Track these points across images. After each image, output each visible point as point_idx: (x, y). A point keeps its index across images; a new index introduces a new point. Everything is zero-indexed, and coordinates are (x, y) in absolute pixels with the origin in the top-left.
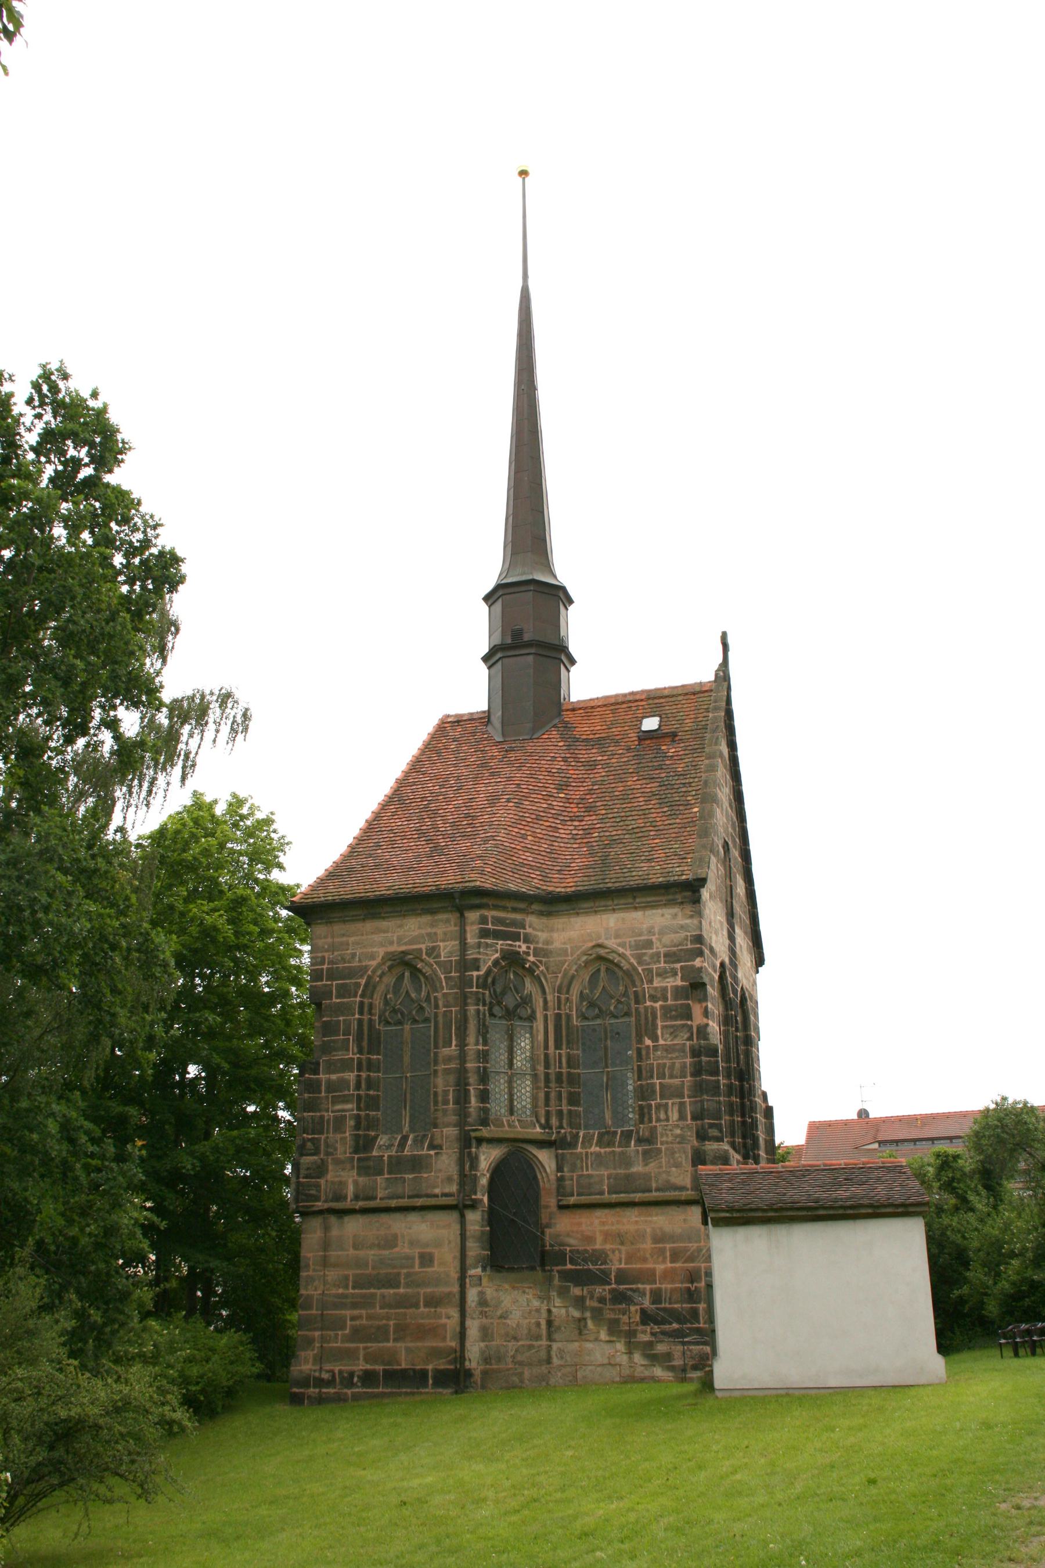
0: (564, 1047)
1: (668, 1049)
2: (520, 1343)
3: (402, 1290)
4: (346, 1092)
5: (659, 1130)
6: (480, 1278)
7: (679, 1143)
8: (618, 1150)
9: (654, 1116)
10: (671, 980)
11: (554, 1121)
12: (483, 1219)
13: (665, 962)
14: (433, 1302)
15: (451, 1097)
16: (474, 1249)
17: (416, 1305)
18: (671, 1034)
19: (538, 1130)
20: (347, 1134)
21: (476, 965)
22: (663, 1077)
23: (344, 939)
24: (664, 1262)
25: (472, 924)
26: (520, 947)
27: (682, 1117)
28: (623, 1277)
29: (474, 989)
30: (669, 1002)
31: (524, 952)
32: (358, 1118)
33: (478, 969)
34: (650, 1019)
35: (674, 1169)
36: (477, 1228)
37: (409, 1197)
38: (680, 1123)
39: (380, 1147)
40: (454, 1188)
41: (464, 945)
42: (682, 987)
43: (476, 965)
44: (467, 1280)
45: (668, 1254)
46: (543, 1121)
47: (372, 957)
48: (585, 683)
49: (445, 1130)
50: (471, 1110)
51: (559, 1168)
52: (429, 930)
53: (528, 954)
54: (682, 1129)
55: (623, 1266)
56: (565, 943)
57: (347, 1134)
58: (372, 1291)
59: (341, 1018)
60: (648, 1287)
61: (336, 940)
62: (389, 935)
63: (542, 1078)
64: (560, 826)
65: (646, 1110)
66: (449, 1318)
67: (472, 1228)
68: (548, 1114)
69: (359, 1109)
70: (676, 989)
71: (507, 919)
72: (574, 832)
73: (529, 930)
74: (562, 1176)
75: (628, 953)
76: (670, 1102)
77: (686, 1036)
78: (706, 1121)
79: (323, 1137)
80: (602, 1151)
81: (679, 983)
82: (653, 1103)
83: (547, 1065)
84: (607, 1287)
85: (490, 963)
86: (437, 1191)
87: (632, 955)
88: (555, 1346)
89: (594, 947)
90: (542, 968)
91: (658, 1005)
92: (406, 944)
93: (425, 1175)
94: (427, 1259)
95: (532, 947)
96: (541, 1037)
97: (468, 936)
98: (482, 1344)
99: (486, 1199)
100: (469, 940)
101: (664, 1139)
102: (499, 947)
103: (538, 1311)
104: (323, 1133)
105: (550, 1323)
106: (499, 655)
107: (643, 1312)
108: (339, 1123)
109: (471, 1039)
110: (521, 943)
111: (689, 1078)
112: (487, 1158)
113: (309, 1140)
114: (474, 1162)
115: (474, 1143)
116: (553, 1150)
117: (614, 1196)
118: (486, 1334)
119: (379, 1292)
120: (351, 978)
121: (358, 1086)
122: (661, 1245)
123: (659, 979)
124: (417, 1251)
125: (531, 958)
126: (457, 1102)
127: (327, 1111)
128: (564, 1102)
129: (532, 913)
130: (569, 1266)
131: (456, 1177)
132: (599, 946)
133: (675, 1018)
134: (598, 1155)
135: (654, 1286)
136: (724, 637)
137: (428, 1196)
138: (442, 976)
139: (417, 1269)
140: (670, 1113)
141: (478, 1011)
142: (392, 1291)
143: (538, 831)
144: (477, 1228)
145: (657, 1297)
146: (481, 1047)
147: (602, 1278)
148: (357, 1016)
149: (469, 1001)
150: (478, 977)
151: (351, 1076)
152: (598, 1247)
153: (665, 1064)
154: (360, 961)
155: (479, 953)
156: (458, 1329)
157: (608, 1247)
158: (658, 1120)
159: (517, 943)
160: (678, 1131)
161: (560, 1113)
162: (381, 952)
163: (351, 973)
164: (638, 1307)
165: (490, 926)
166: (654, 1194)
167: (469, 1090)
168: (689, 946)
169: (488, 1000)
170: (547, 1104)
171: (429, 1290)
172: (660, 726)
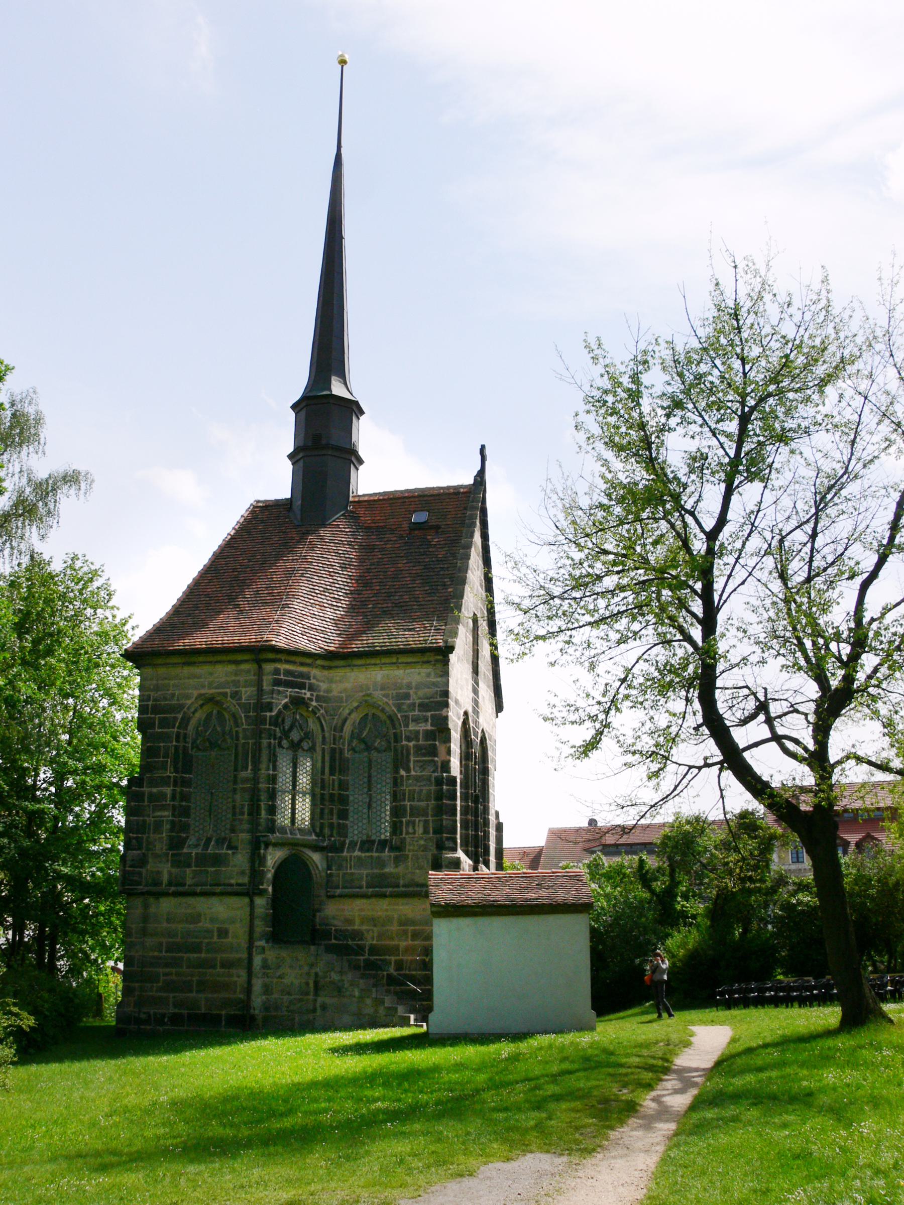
1: (417, 779)
3: (203, 955)
5: (408, 840)
6: (263, 948)
8: (375, 854)
12: (268, 904)
14: (227, 965)
15: (246, 810)
16: (260, 927)
17: (214, 967)
18: (421, 767)
19: (314, 837)
23: (166, 682)
24: (406, 940)
26: (305, 694)
27: (426, 831)
28: (374, 950)
31: (309, 699)
33: (271, 710)
39: (189, 846)
40: (245, 880)
42: (432, 731)
46: (318, 830)
52: (234, 678)
53: (311, 700)
54: (426, 840)
55: (374, 942)
59: (162, 745)
61: (160, 682)
65: (398, 825)
68: (322, 825)
69: (173, 815)
73: (313, 681)
75: (391, 702)
76: (417, 820)
79: (145, 836)
80: (363, 855)
81: (429, 727)
82: (404, 820)
83: (323, 788)
84: (362, 958)
85: (280, 707)
86: (233, 881)
87: (394, 704)
91: (411, 744)
96: (319, 765)
97: (265, 684)
99: (270, 889)
100: (265, 688)
106: (301, 455)
109: (263, 766)
112: (273, 857)
114: (263, 860)
115: (263, 846)
118: (267, 990)
121: (173, 798)
125: (314, 703)
127: (149, 816)
128: (335, 817)
130: (333, 941)
131: (247, 872)
133: (424, 755)
134: (359, 858)
136: (483, 449)
137: (224, 885)
142: (196, 955)
144: (262, 910)
145: (399, 966)
149: (263, 735)
150: (271, 717)
151: (168, 790)
152: (356, 927)
153: (414, 791)
154: (178, 700)
157: (364, 928)
158: (408, 833)
159: (303, 691)
160: (422, 842)
162: (195, 693)
165: (282, 677)
168: (439, 699)
170: (322, 817)
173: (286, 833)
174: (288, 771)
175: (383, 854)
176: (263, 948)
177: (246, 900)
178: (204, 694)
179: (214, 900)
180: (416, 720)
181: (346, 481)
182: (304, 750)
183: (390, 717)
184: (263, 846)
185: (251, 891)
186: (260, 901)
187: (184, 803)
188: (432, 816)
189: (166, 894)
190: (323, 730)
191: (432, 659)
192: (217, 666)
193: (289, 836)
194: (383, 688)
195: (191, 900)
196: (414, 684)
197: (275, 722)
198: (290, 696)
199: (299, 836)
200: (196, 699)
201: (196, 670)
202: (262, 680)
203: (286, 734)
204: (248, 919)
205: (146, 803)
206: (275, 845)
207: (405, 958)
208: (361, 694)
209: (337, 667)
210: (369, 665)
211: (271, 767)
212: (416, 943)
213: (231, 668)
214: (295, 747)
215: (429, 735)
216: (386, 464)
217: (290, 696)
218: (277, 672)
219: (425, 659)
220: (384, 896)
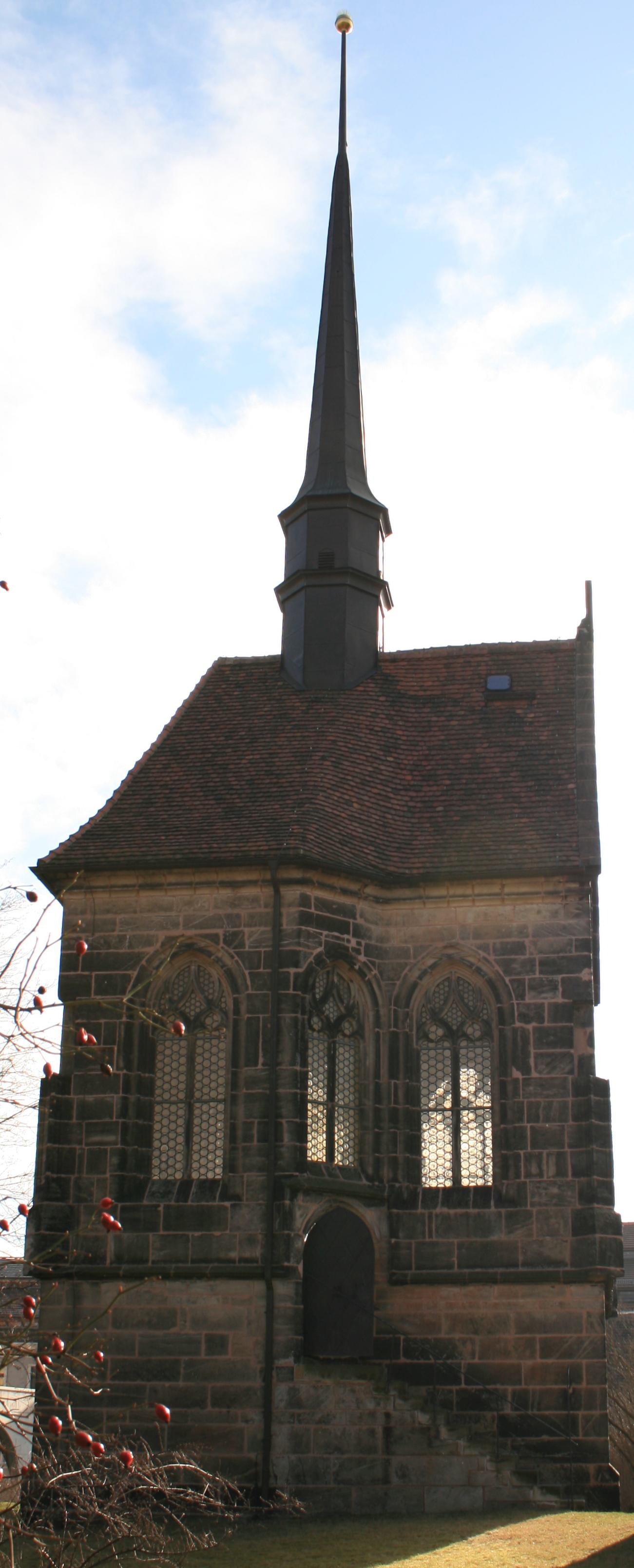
0: (401, 1076)
1: (543, 1084)
2: (345, 1456)
3: (181, 1384)
4: (107, 1120)
5: (529, 1188)
6: (291, 1370)
7: (556, 1205)
8: (472, 1211)
9: (522, 1169)
10: (550, 995)
11: (386, 1172)
12: (297, 1294)
13: (541, 972)
14: (225, 1400)
15: (255, 1132)
16: (285, 1334)
17: (201, 1404)
18: (548, 1065)
19: (364, 1182)
20: (108, 1175)
21: (294, 959)
22: (537, 1120)
23: (109, 916)
24: (532, 1356)
25: (290, 905)
26: (348, 941)
27: (560, 1172)
28: (475, 1373)
29: (291, 991)
30: (546, 1024)
31: (354, 949)
32: (123, 1155)
33: (296, 965)
34: (520, 1043)
35: (548, 1238)
36: (289, 1304)
37: (193, 1261)
38: (557, 1179)
39: (153, 1194)
40: (257, 1252)
41: (278, 933)
42: (564, 1005)
43: (294, 959)
44: (274, 1373)
45: (538, 1347)
46: (370, 1171)
47: (149, 942)
48: (400, 631)
49: (245, 1175)
50: (283, 1150)
51: (393, 1233)
52: (229, 911)
53: (358, 951)
54: (560, 1187)
55: (476, 1360)
56: (406, 942)
57: (108, 1175)
58: (139, 1382)
59: (102, 1021)
60: (510, 1388)
61: (98, 917)
62: (173, 914)
63: (371, 1115)
64: (392, 795)
65: (511, 1162)
66: (247, 1421)
67: (282, 1304)
68: (378, 1163)
69: (124, 1141)
70: (556, 1007)
71: (334, 903)
72: (410, 804)
73: (359, 921)
74: (396, 1243)
75: (492, 958)
76: (545, 1152)
77: (567, 1068)
78: (595, 1177)
79: (73, 1177)
80: (452, 1212)
81: (560, 1000)
82: (522, 1152)
83: (378, 1099)
84: (454, 1388)
85: (311, 959)
86: (233, 1255)
87: (497, 961)
88: (395, 1461)
89: (445, 947)
90: (375, 972)
91: (530, 1027)
92: (196, 927)
93: (217, 1233)
94: (217, 1344)
95: (363, 943)
96: (370, 1062)
97: (284, 921)
98: (293, 1457)
99: (300, 1268)
100: (285, 927)
101: (536, 1199)
102: (323, 938)
103: (372, 1414)
104: (73, 1173)
105: (388, 1431)
106: (302, 583)
107: (503, 1419)
108: (96, 1160)
109: (286, 1056)
110: (350, 937)
111: (571, 1123)
112: (306, 1212)
113: (54, 1180)
114: (288, 1218)
115: (288, 1192)
116: (384, 1209)
117: (466, 1271)
118: (298, 1443)
119: (149, 1384)
120: (117, 969)
121: (124, 1113)
122: (528, 1335)
123: (533, 993)
124: (204, 1332)
125: (362, 958)
126: (263, 1138)
127: (80, 1143)
128: (400, 1147)
129: (366, 899)
130: (403, 1360)
131: (260, 1237)
132: (451, 946)
133: (553, 1044)
134: (446, 1218)
135: (517, 1387)
136: (588, 585)
137: (219, 1260)
138: (247, 972)
139: (203, 1356)
140: (545, 1168)
141: (295, 1020)
142: (167, 1384)
143: (366, 798)
144: (289, 1304)
145: (521, 1400)
146: (298, 1068)
147: (451, 1375)
148: (124, 1019)
149: (283, 1006)
150: (297, 975)
151: (115, 1099)
152: (442, 1335)
153: (538, 1103)
154: (131, 946)
155: (299, 944)
156: (260, 1436)
157: (457, 1336)
158: (528, 1175)
159: (346, 936)
160: (555, 1190)
161: (394, 1162)
162: (162, 935)
163: (119, 962)
164: (495, 1413)
165: (313, 910)
166: (521, 1269)
167: (281, 1124)
168: (574, 953)
169: (308, 1008)
170: (377, 1149)
171: (220, 1384)
172: (511, 686)
173: (323, 1175)
174: (321, 1069)
175: (486, 1210)
176: (291, 1370)
177: (259, 1287)
178: (175, 938)
179: (199, 1287)
180: (537, 987)
181: (370, 629)
182: (345, 1035)
183: (491, 983)
184: (288, 1192)
185: (268, 1270)
186: (284, 1289)
187: (140, 1122)
188: (571, 1146)
189: (113, 1276)
190: (375, 1002)
191: (561, 888)
192: (199, 892)
193: (327, 1178)
194: (477, 935)
195: (157, 1286)
196: (530, 930)
197: (305, 983)
198: (327, 942)
199: (342, 1179)
200: (163, 944)
201: (157, 896)
202: (280, 915)
203: (318, 1006)
204: (263, 1321)
205: (74, 1121)
206: (307, 1192)
207: (531, 1387)
208: (440, 945)
209: (398, 900)
210: (454, 896)
211: (299, 1060)
212: (550, 1361)
213: (226, 893)
214: (332, 1028)
215: (558, 1012)
216: (427, 606)
217: (327, 942)
218: (304, 901)
219: (551, 888)
220: (492, 1280)
